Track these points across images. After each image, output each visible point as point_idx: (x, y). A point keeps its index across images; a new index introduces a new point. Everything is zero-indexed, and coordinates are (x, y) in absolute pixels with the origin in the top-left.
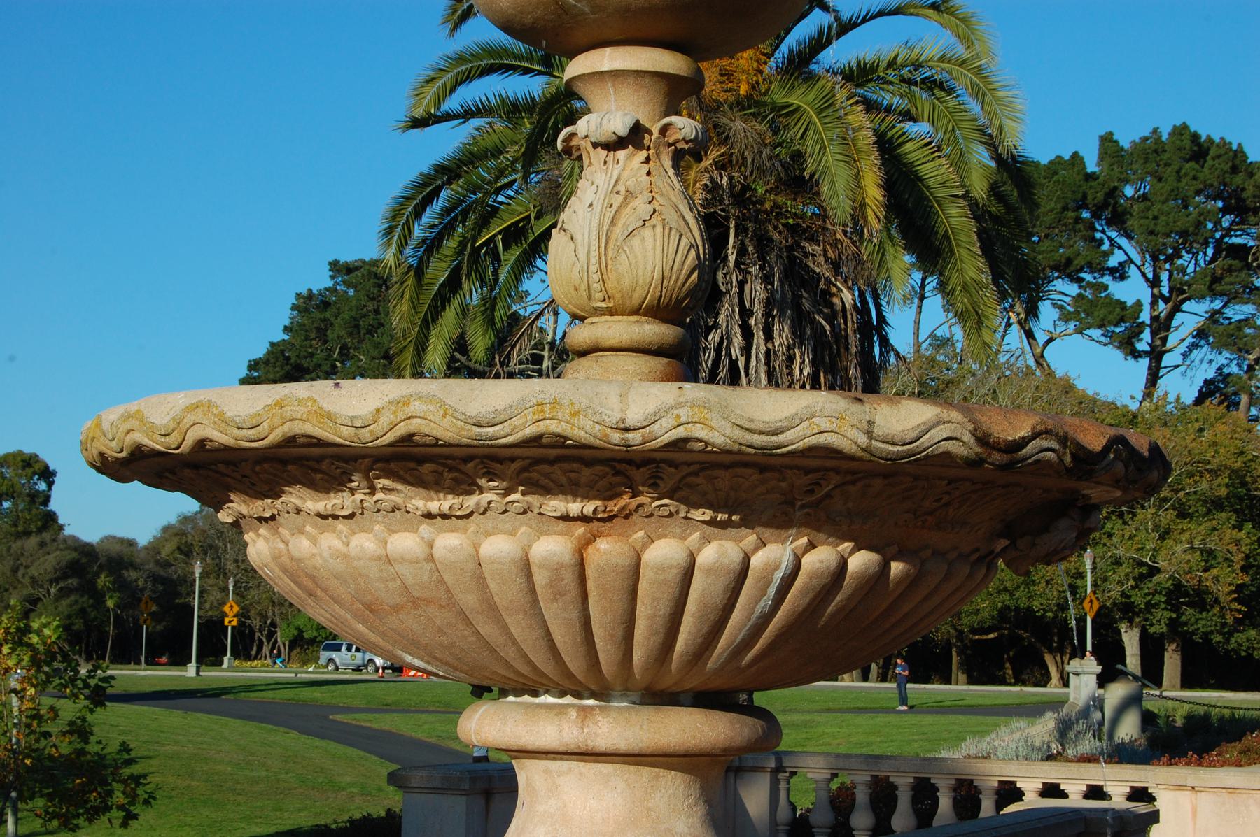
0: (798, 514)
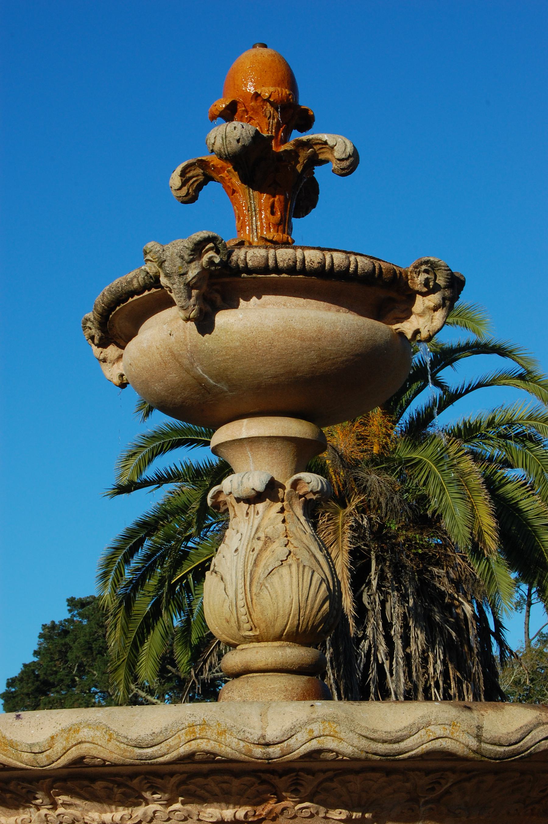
0: (422, 809)
